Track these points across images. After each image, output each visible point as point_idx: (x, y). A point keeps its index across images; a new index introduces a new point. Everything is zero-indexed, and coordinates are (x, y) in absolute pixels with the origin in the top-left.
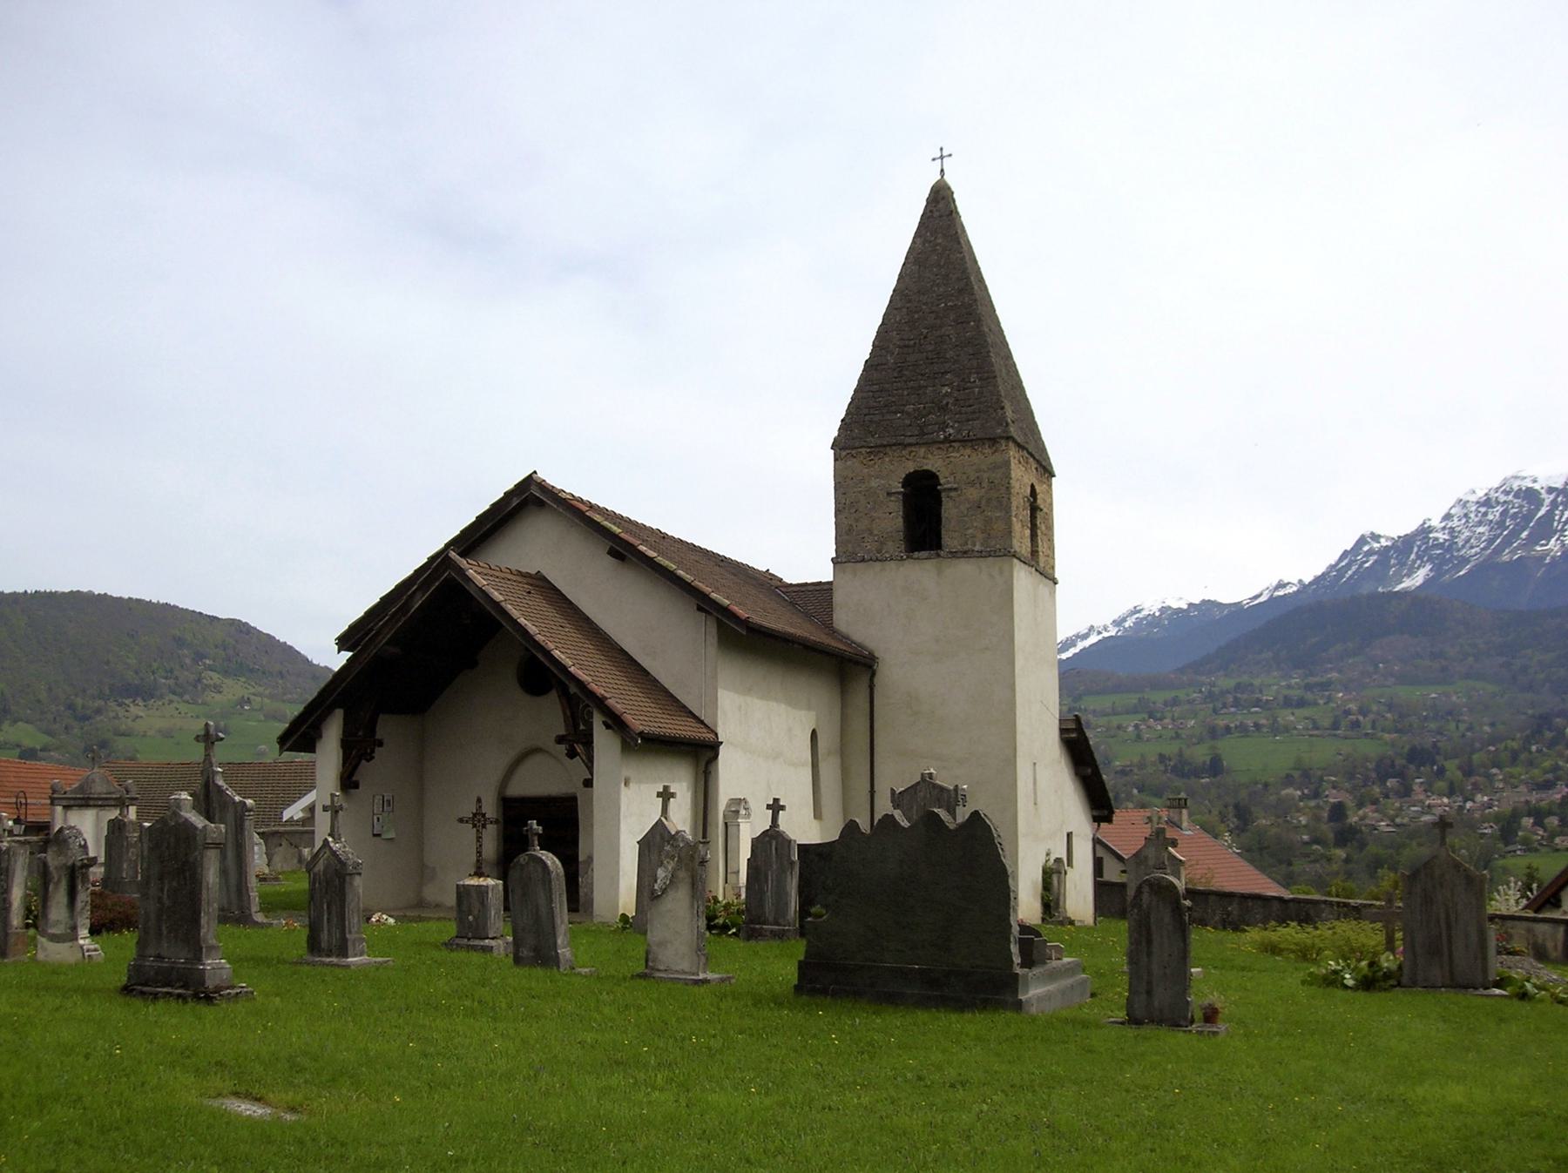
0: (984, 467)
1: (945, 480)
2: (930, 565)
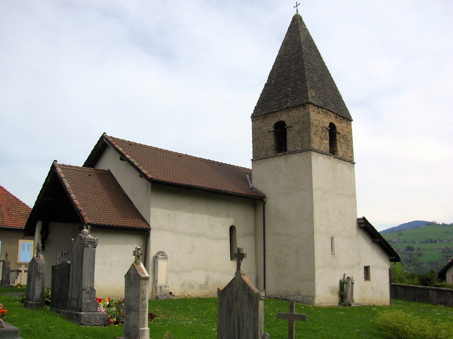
0: (301, 116)
1: (288, 124)
2: (283, 158)
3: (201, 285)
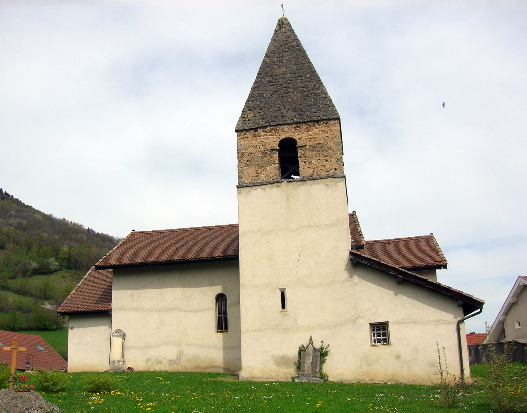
1: (300, 143)
3: (170, 361)
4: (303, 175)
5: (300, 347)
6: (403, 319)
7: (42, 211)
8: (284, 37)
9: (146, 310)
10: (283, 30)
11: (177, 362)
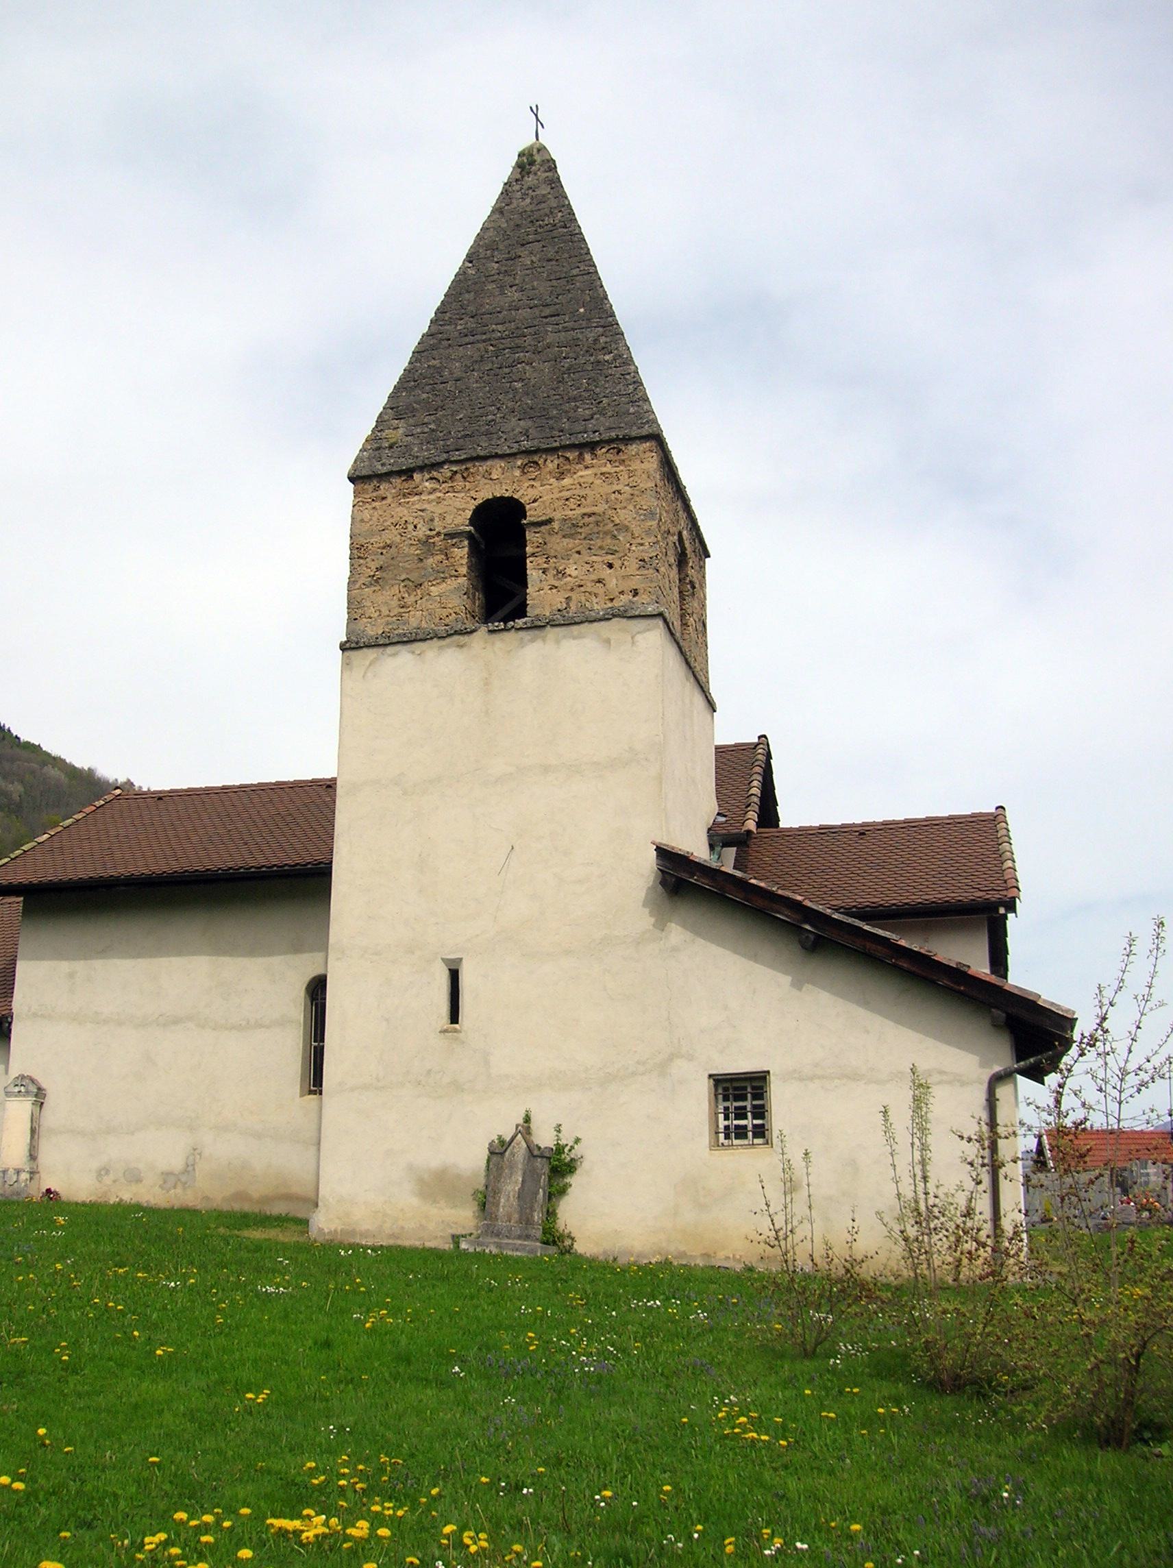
3: (166, 1175)
4: (536, 612)
5: (491, 1144)
6: (816, 1065)
7: (69, 759)
8: (528, 201)
9: (106, 1022)
10: (530, 180)
11: (183, 1179)
